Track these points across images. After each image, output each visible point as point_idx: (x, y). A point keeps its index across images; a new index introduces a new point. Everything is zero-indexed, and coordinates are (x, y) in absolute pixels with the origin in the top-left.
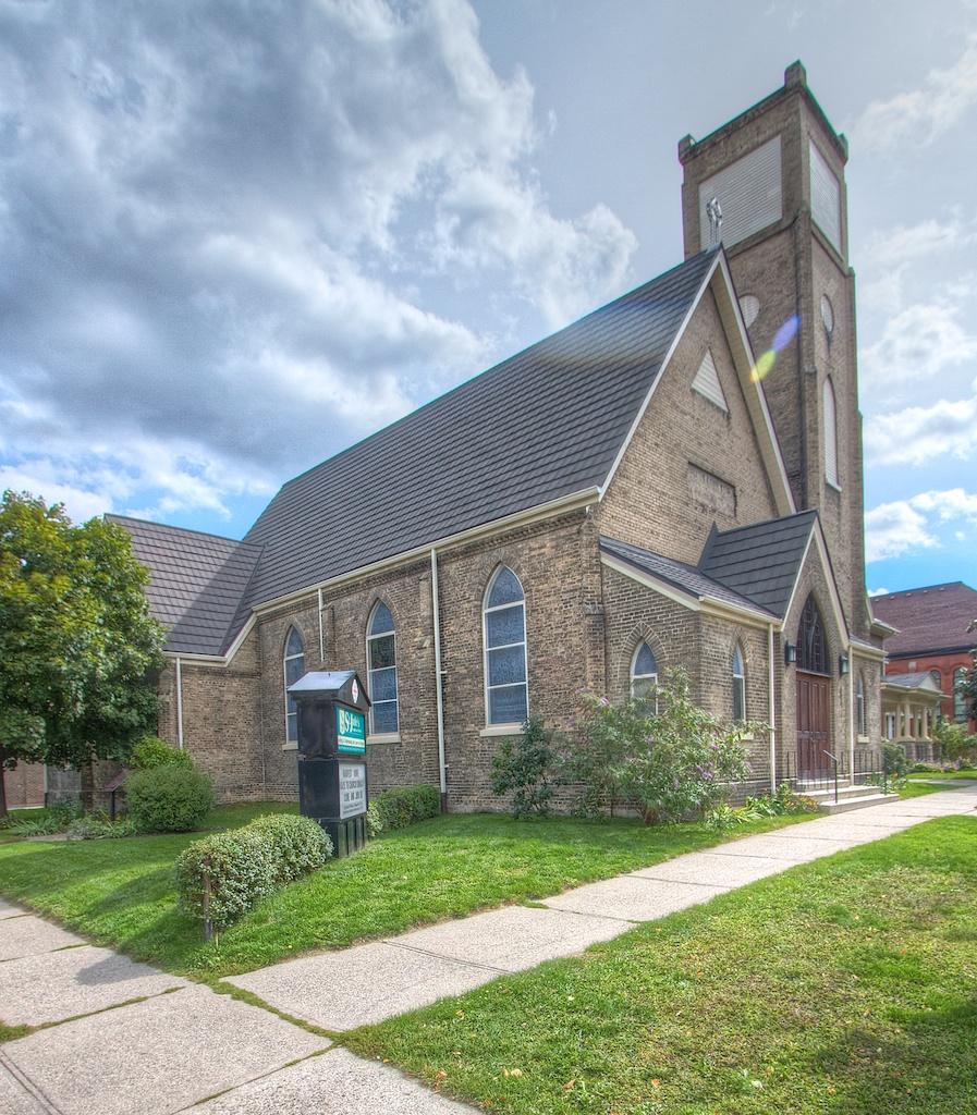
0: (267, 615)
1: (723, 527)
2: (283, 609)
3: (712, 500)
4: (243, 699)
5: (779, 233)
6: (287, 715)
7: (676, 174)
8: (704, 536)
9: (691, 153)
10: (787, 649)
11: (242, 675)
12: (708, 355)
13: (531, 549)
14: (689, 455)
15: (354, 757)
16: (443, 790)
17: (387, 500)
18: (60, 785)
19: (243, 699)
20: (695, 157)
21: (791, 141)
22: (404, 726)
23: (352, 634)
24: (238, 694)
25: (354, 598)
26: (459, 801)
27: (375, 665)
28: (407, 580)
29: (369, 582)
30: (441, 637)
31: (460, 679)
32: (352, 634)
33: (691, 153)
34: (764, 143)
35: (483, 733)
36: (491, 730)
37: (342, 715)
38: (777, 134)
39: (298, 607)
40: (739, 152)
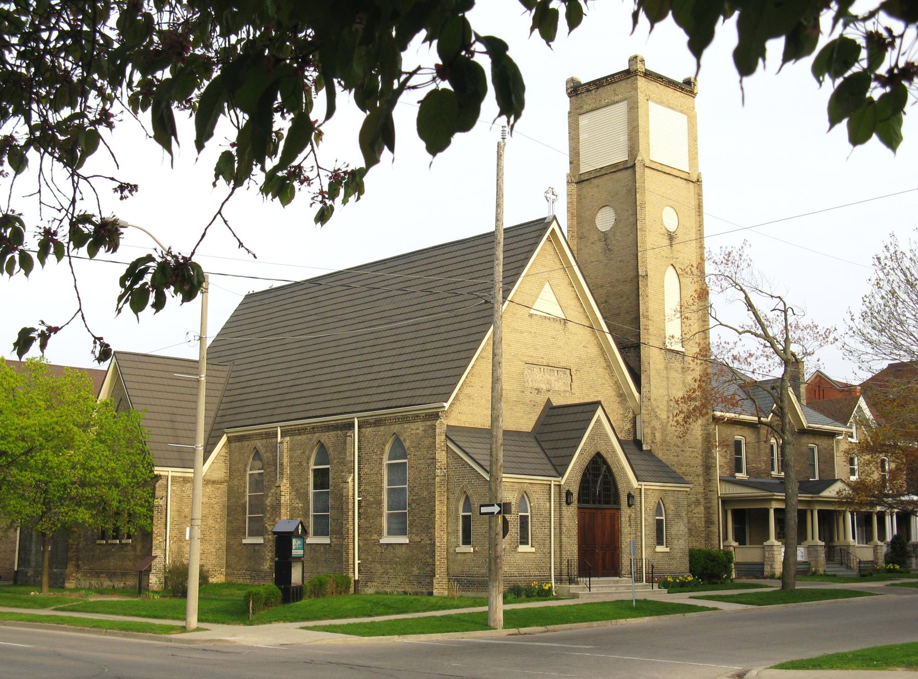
0: (237, 437)
1: (556, 402)
2: (250, 435)
3: (549, 383)
4: (214, 501)
5: (627, 168)
6: (248, 515)
7: (565, 102)
8: (539, 410)
9: (575, 90)
10: (569, 494)
11: (214, 482)
12: (547, 286)
13: (412, 429)
14: (525, 359)
15: (298, 559)
16: (357, 578)
17: (328, 357)
18: (33, 564)
19: (214, 501)
20: (577, 95)
21: (633, 107)
22: (334, 532)
23: (300, 463)
24: (209, 498)
25: (304, 437)
26: (366, 586)
27: (315, 488)
28: (339, 432)
29: (314, 429)
30: (359, 474)
31: (369, 504)
32: (300, 463)
33: (575, 90)
34: (617, 102)
35: (381, 541)
36: (386, 540)
37: (294, 541)
38: (626, 99)
39: (260, 436)
40: (603, 103)
